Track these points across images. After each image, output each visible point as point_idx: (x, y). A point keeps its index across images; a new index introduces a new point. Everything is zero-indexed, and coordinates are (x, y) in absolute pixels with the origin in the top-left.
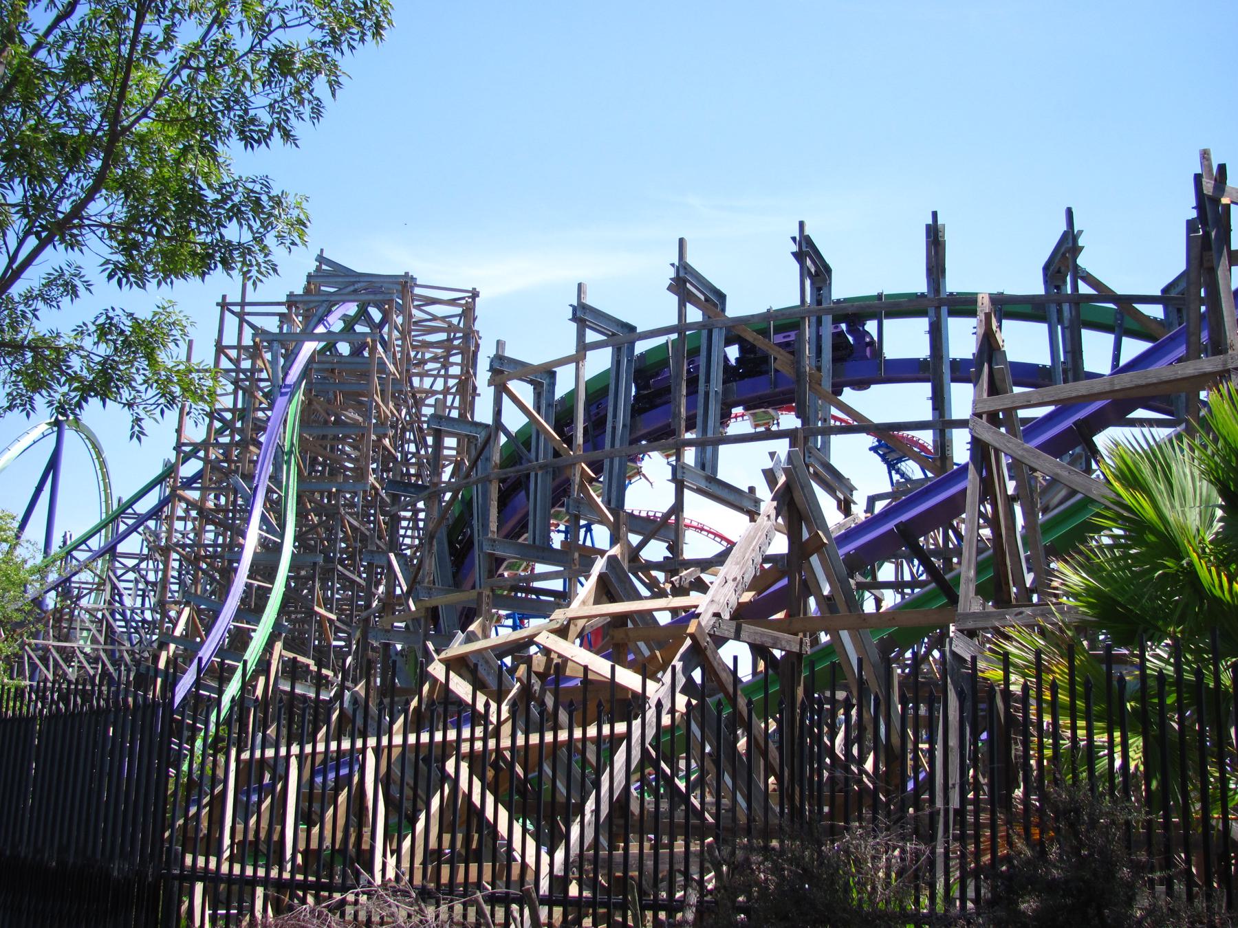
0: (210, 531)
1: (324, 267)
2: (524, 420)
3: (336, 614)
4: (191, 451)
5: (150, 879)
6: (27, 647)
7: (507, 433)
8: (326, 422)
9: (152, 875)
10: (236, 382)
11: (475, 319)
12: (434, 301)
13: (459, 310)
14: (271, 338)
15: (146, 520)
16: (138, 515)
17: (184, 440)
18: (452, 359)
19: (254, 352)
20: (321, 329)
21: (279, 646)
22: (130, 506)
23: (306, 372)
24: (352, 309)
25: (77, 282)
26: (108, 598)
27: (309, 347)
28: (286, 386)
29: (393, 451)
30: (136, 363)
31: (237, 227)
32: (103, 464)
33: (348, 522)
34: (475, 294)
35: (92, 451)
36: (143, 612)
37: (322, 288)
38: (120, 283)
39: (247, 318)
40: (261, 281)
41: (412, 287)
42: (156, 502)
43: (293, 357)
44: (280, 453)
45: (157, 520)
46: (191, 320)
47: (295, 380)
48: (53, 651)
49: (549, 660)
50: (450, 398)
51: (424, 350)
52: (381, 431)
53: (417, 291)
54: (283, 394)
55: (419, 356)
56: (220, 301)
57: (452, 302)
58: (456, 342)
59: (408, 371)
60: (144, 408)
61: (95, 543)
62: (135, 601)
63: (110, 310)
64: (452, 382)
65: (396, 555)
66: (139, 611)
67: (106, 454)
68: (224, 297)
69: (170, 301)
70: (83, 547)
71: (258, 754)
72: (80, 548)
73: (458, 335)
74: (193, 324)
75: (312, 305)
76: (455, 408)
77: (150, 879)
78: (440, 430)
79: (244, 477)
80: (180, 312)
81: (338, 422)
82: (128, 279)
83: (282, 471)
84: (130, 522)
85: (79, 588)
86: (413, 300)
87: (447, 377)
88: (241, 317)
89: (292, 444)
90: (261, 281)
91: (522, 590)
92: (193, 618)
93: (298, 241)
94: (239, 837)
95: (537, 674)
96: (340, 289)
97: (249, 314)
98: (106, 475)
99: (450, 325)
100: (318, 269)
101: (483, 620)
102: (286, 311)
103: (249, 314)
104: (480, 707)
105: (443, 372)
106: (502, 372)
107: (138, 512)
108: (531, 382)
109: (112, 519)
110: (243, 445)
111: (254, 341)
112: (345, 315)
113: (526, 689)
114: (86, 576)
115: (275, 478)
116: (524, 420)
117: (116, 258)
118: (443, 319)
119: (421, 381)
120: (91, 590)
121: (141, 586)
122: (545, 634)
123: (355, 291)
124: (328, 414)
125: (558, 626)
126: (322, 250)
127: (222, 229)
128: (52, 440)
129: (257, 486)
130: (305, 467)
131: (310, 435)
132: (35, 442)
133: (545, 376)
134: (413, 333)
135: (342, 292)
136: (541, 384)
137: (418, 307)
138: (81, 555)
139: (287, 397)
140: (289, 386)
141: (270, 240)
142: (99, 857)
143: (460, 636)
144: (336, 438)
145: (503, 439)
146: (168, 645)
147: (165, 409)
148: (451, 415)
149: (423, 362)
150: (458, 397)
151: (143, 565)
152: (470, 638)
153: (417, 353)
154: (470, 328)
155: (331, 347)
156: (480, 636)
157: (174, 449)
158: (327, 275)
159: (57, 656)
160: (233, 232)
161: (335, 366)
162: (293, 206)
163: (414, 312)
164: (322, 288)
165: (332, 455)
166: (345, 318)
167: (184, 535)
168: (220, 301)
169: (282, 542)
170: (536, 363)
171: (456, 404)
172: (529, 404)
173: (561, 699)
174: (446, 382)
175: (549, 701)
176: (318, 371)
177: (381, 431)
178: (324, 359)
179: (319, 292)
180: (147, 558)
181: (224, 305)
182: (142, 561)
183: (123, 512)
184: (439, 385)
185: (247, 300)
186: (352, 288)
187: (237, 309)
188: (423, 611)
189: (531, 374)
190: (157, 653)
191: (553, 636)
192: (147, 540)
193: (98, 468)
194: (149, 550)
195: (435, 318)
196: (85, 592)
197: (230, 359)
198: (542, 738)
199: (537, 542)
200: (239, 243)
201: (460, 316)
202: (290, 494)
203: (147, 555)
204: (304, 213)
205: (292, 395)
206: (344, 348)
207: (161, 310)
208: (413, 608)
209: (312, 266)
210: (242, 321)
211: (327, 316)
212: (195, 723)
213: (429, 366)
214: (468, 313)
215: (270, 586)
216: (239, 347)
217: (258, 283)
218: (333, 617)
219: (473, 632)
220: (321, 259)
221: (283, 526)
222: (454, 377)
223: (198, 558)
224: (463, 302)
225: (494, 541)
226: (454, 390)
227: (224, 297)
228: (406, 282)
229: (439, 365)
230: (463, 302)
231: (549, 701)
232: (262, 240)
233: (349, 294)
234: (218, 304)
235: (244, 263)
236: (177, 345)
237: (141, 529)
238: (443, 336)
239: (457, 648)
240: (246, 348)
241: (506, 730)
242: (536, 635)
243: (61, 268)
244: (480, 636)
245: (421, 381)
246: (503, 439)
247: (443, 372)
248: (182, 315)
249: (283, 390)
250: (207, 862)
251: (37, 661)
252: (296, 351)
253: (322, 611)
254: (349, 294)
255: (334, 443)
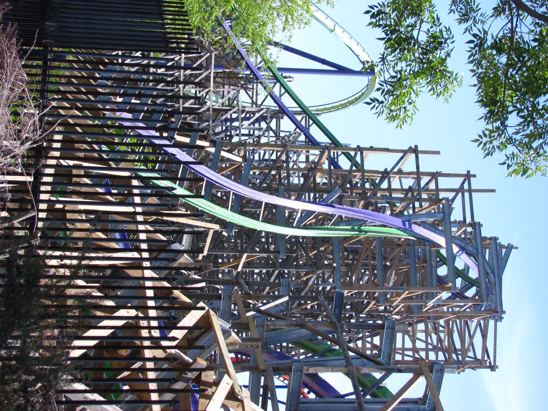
0: (299, 180)
1: (504, 250)
2: (394, 391)
3: (242, 271)
4: (356, 162)
5: (44, 41)
6: (209, 54)
7: (383, 379)
8: (385, 259)
9: (47, 42)
10: (410, 189)
11: (473, 368)
12: (484, 336)
13: (479, 356)
14: (446, 211)
15: (305, 134)
16: (309, 129)
17: (365, 153)
18: (441, 354)
19: (435, 200)
20: (455, 249)
21: (217, 227)
22: (314, 122)
23: (422, 240)
24: (473, 274)
25: (470, 22)
26: (247, 109)
27: (441, 240)
28: (410, 225)
29: (367, 310)
30: (414, 64)
31: (518, 123)
32: (344, 106)
33: (312, 277)
34: (493, 368)
35: (354, 98)
36: (237, 135)
37: (488, 250)
38: (471, 42)
39: (460, 194)
40: (479, 145)
41: (494, 318)
42: (319, 140)
43: (433, 229)
44: (360, 224)
45: (305, 142)
46: (449, 99)
47: (415, 231)
48: (207, 72)
49: (210, 385)
50: (410, 353)
51: (446, 332)
52: (382, 299)
53: (492, 322)
54: (404, 223)
55: (441, 329)
56: (471, 173)
57: (485, 350)
58: (454, 356)
59: (429, 318)
60: (381, 70)
61: (287, 101)
62: (245, 128)
63: (452, 40)
64: (423, 354)
65: (287, 302)
66: (238, 132)
67: (352, 108)
68: (474, 176)
69: (461, 81)
70: (283, 90)
71: (136, 191)
72: (282, 88)
73: (460, 357)
74: (447, 100)
75: (474, 242)
76: (403, 358)
77: (44, 41)
78: (383, 329)
79: (341, 198)
80: (454, 91)
81: (386, 267)
82: (474, 48)
83: (346, 225)
84: (303, 123)
85: (253, 88)
86: (484, 319)
87: (427, 350)
88: (460, 190)
89: (366, 232)
90: (479, 145)
91: (265, 393)
92: (234, 165)
93: (511, 169)
94: (75, 172)
95: (200, 376)
96: (488, 263)
97: (463, 196)
98: (336, 108)
99: (468, 350)
100: (502, 246)
101: (240, 343)
102: (467, 222)
103: (463, 196)
104: (174, 333)
105: (430, 347)
106: (431, 372)
107: (310, 128)
108: (425, 396)
109: (304, 111)
110: (363, 195)
111: (443, 199)
112: (469, 267)
113: (187, 367)
114: (262, 94)
115: (340, 220)
116: (394, 391)
117: (489, 37)
118: (472, 344)
119: (422, 331)
120: (252, 98)
121: (257, 133)
122: (231, 382)
123: (487, 274)
124: (391, 260)
125: (237, 391)
126: (517, 248)
127: (516, 112)
128: (358, 67)
129: (334, 207)
130: (350, 244)
131: (374, 247)
132: (357, 56)
133: (432, 407)
134: (458, 321)
135: (486, 264)
136: (424, 403)
137: (479, 324)
138: (277, 90)
139: (402, 226)
140: (410, 227)
141: (511, 149)
142: (60, 15)
143: (227, 326)
144: (374, 267)
145: (378, 375)
146: (214, 146)
147: (381, 91)
148: (397, 355)
149: (437, 332)
150: (411, 359)
151: (271, 134)
152: (226, 333)
153: (443, 327)
154: (466, 364)
155: (443, 261)
156: (228, 341)
157: (358, 146)
158: (498, 253)
159: (203, 76)
160: (513, 120)
161: (429, 263)
162: (538, 164)
163: (475, 321)
164: (488, 250)
165: (360, 264)
166: (467, 268)
167: (295, 162)
168: (471, 173)
169: (293, 227)
170: (440, 397)
171: (406, 358)
172: (407, 395)
173: (181, 395)
174: (422, 350)
175: (179, 385)
176: (424, 251)
177: (382, 299)
178: (434, 255)
179: (484, 248)
180: (277, 135)
181: (468, 176)
182: (276, 134)
183: (310, 117)
184: (420, 345)
185: (473, 194)
186: (489, 271)
187: (466, 186)
188: (246, 321)
189: (431, 393)
190: (208, 139)
191: (228, 388)
192: (291, 135)
193: (342, 103)
194: (283, 138)
195: (471, 337)
196: (250, 93)
197: (427, 184)
198: (150, 298)
199: (302, 405)
200: (507, 126)
201: (475, 357)
202: (330, 232)
203: (279, 136)
204: (532, 174)
205: (404, 230)
206: (442, 271)
207: (454, 77)
208: (248, 314)
209: (503, 241)
210: (457, 191)
211: (467, 253)
212: (159, 162)
213: (434, 337)
214: (478, 364)
215: (260, 220)
216: (437, 190)
217: (477, 143)
218: (240, 269)
219: (230, 335)
220: (510, 248)
221: (306, 227)
222: (427, 355)
223: (279, 169)
224: (486, 358)
225: (301, 371)
226: (417, 356)
227: (474, 176)
228: (497, 312)
229: (435, 344)
230: (486, 358)
231: (179, 385)
232: (510, 144)
233: (485, 269)
234: (468, 172)
235: (491, 131)
236: (430, 90)
237: (298, 130)
238: (458, 345)
239: (218, 323)
240: (438, 195)
241: (159, 354)
242: (229, 376)
243: (480, 9)
244: (228, 341)
245: (422, 331)
246: (378, 375)
247: (430, 347)
248: (452, 91)
249: (407, 223)
250: (56, 149)
251: (199, 62)
252: (437, 231)
253: (243, 260)
254: (485, 269)
255: (370, 267)
